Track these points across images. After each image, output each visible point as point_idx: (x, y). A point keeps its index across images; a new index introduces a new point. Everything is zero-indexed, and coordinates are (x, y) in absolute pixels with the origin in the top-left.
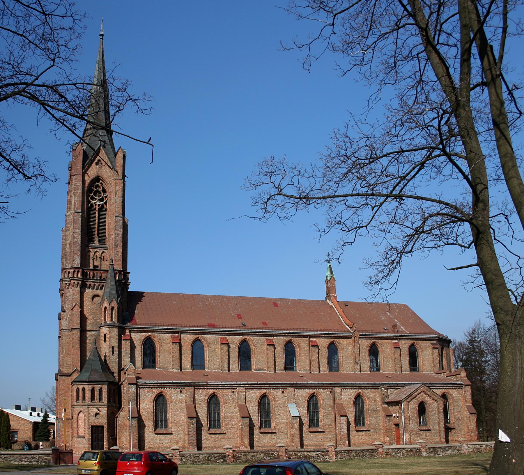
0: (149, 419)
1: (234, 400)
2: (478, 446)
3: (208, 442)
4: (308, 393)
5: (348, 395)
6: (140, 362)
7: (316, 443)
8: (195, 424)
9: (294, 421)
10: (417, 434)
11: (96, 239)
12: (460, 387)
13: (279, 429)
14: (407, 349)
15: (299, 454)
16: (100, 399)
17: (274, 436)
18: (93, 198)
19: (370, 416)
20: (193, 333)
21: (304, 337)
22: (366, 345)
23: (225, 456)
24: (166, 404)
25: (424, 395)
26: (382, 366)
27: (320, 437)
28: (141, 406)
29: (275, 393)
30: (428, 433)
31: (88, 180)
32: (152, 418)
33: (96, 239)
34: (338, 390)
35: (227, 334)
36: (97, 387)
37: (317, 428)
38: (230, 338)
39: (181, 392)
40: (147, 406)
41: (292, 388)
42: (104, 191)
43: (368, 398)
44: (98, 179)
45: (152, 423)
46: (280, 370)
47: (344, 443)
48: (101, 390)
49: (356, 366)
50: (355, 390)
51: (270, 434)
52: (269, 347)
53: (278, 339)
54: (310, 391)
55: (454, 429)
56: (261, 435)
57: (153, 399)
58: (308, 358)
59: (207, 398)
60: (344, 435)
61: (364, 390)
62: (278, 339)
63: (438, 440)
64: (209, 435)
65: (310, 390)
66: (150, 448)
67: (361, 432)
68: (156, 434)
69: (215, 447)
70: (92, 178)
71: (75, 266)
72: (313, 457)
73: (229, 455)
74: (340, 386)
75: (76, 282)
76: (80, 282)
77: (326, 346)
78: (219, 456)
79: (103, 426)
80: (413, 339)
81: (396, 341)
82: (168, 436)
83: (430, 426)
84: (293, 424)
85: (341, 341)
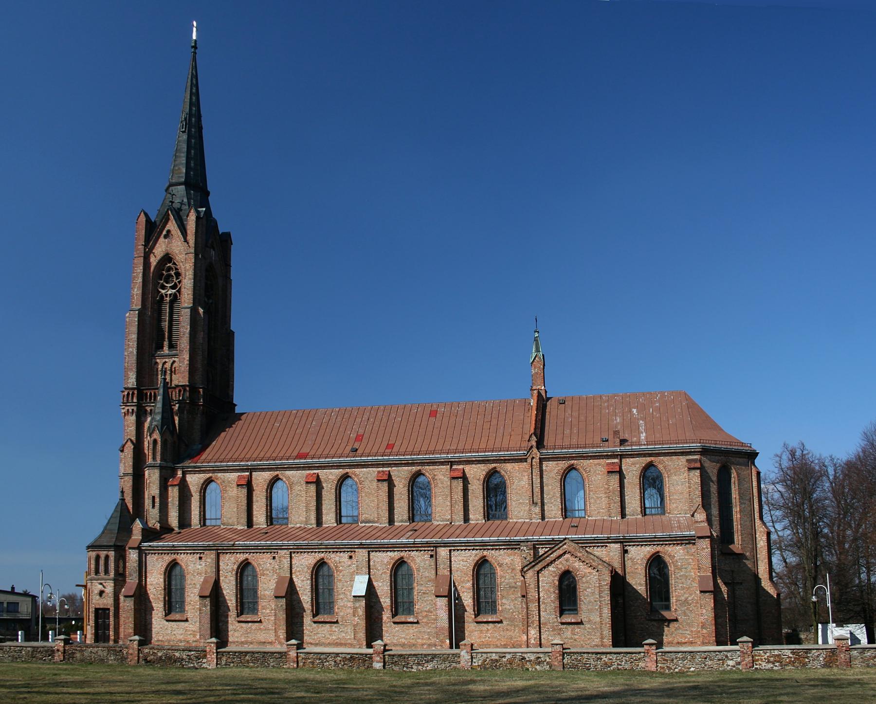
0: (158, 598)
1: (274, 571)
2: (494, 657)
3: (236, 634)
4: (392, 559)
5: (463, 560)
6: (198, 517)
7: (403, 640)
8: (209, 607)
9: (357, 605)
10: (554, 630)
11: (166, 343)
12: (689, 541)
13: (342, 617)
14: (638, 473)
15: (160, 654)
16: (107, 572)
17: (334, 627)
18: (163, 287)
19: (503, 597)
20: (270, 469)
21: (442, 463)
22: (556, 471)
23: (53, 651)
24: (331, 576)
25: (572, 559)
26: (669, 505)
27: (411, 631)
28: (148, 580)
29: (337, 559)
30: (577, 629)
31: (154, 261)
32: (162, 597)
33: (166, 343)
34: (443, 552)
35: (318, 468)
36: (103, 554)
37: (408, 617)
38: (394, 471)
39: (200, 558)
40: (155, 581)
41: (364, 550)
42: (178, 275)
43: (501, 565)
44: (167, 258)
45: (161, 605)
46: (402, 521)
47: (443, 642)
48: (107, 557)
49: (533, 508)
50: (474, 552)
51: (328, 625)
52: (380, 484)
53: (398, 471)
54: (396, 555)
55: (676, 620)
56: (315, 625)
57: (163, 569)
58: (449, 499)
59: (235, 567)
60: (442, 628)
61: (493, 552)
62: (398, 471)
63: (597, 641)
64: (237, 624)
65: (396, 553)
66: (158, 641)
67: (486, 625)
68: (167, 621)
69: (246, 642)
70: (159, 258)
71: (130, 386)
72: (182, 659)
73: (58, 650)
74: (445, 545)
75: (130, 409)
76: (135, 408)
77: (482, 477)
78: (47, 651)
79: (109, 609)
80: (650, 455)
81: (616, 461)
82: (183, 623)
83: (583, 616)
84: (355, 609)
85: (509, 466)
